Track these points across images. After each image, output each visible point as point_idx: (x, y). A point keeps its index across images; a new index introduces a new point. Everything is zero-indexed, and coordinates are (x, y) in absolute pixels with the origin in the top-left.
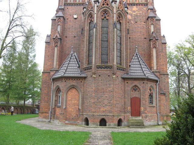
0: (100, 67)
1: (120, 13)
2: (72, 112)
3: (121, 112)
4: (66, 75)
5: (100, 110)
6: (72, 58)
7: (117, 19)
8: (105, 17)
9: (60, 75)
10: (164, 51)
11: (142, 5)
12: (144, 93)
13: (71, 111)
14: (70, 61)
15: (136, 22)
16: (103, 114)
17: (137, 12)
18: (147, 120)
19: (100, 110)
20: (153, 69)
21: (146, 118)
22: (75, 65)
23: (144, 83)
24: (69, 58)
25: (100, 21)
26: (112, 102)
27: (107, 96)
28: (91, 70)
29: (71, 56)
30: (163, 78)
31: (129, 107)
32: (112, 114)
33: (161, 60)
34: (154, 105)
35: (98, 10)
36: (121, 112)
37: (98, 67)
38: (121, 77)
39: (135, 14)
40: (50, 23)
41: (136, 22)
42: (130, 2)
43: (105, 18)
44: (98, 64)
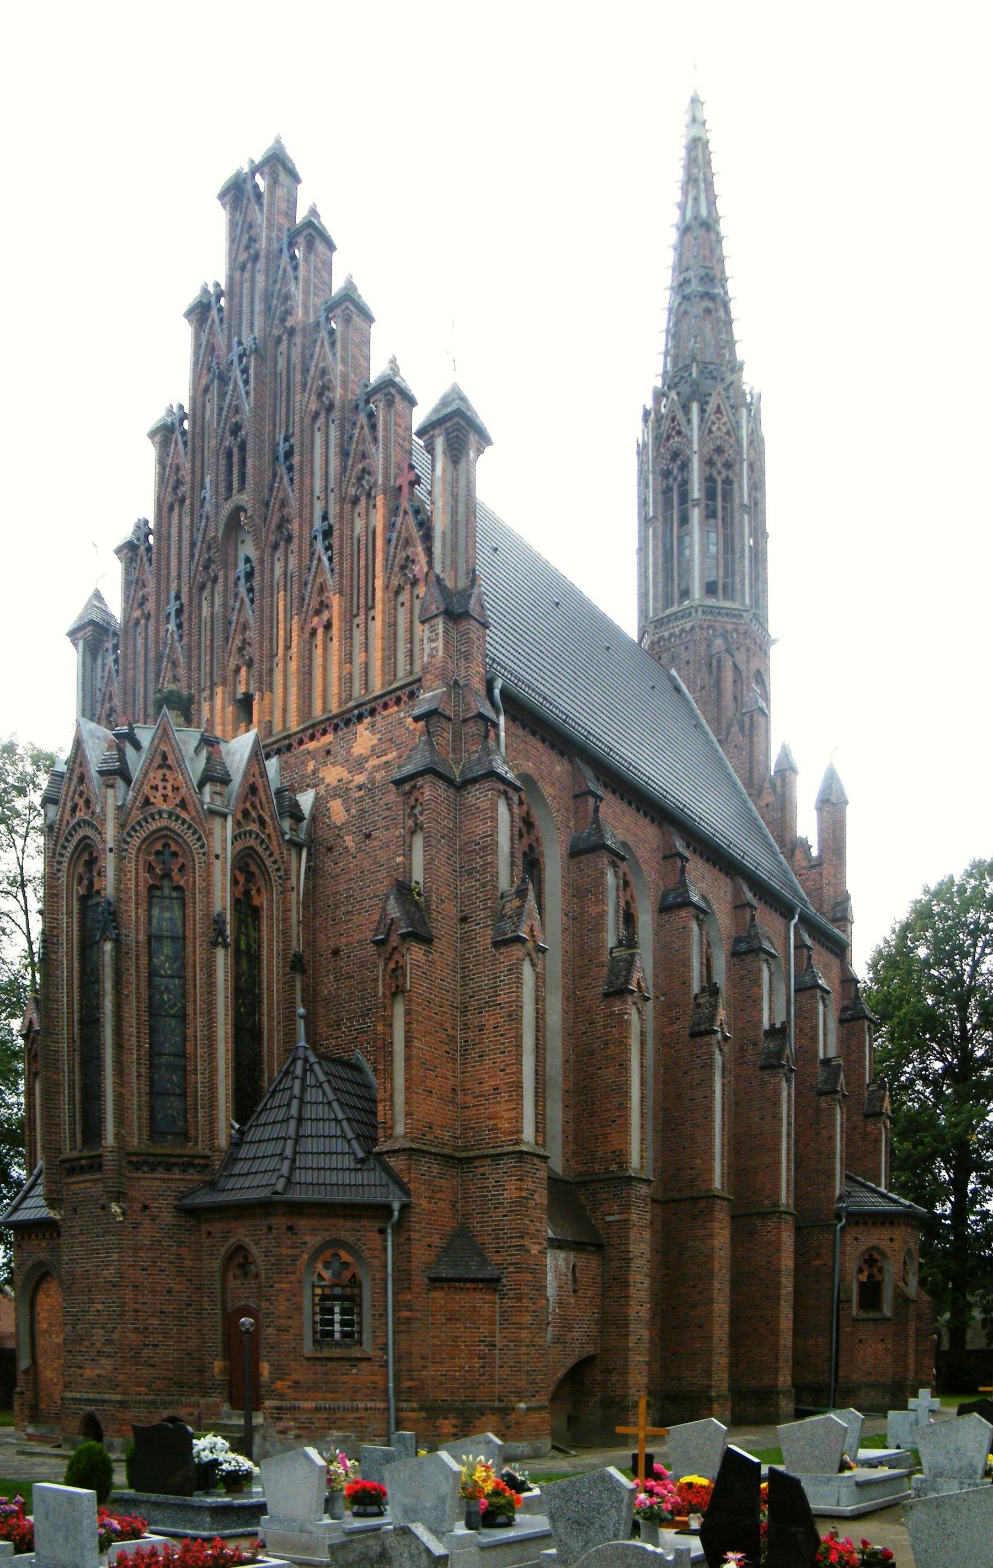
0: (145, 1163)
1: (251, 848)
2: (55, 1385)
3: (180, 1385)
4: (297, 1195)
5: (82, 1375)
6: (310, 1095)
7: (143, 875)
8: (167, 875)
9: (264, 1194)
10: (503, 998)
11: (398, 701)
12: (272, 1286)
13: (51, 1380)
14: (300, 1120)
15: (368, 836)
16: (91, 1396)
17: (374, 762)
18: (283, 1432)
19: (82, 1375)
20: (390, 1137)
21: (280, 1419)
22: (333, 1129)
23: (270, 1228)
24: (295, 1103)
25: (69, 913)
26: (116, 1336)
27: (100, 1307)
28: (98, 1176)
29: (303, 1089)
30: (491, 1183)
31: (216, 1363)
32: (118, 1397)
33: (487, 1062)
34: (368, 1347)
35: (55, 850)
36: (180, 1385)
37: (134, 1159)
38: (176, 1207)
39: (360, 779)
40: (849, 798)
41: (368, 836)
42: (285, 728)
43: (166, 883)
44: (68, 1154)
